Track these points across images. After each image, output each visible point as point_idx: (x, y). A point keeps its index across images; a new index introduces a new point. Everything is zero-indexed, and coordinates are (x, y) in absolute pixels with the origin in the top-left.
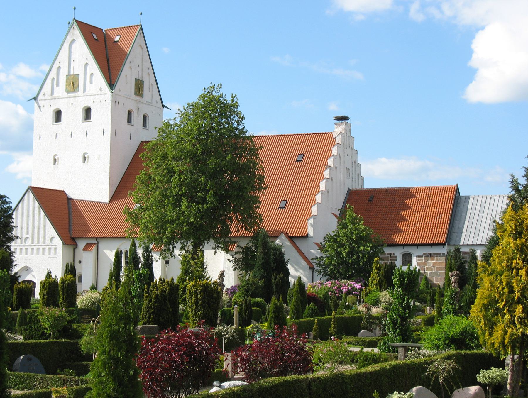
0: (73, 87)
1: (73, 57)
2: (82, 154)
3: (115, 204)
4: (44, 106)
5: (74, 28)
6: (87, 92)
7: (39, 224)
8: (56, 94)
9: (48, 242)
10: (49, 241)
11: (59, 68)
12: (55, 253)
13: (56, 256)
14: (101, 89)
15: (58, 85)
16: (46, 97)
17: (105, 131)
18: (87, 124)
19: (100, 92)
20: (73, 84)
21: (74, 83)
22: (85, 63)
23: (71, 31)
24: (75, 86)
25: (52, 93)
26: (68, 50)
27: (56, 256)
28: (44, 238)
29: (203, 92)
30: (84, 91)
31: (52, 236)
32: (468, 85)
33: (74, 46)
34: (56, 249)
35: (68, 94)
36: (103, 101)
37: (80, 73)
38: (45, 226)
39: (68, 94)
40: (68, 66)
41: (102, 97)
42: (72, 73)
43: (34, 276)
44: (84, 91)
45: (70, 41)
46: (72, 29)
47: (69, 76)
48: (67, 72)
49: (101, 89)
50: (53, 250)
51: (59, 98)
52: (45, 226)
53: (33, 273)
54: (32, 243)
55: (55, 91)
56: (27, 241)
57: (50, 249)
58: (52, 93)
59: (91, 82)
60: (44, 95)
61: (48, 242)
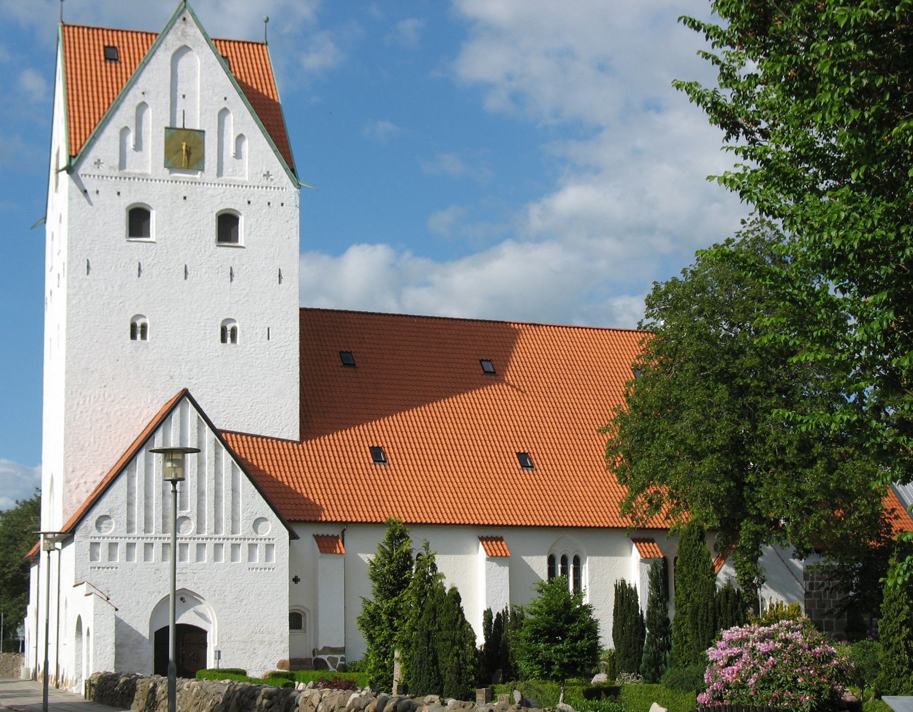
0: (189, 159)
1: (181, 89)
2: (220, 322)
3: (310, 444)
4: (97, 192)
5: (184, 19)
6: (226, 177)
7: (218, 484)
8: (130, 168)
9: (244, 528)
10: (251, 529)
11: (142, 106)
12: (268, 557)
13: (269, 564)
14: (267, 175)
15: (138, 146)
16: (104, 169)
17: (91, 265)
18: (138, 244)
19: (265, 182)
20: (188, 153)
21: (192, 151)
22: (222, 107)
23: (177, 25)
24: (193, 156)
25: (122, 165)
26: (169, 68)
27: (112, 563)
28: (234, 520)
29: (740, 227)
30: (220, 173)
31: (258, 516)
32: (359, 242)
33: (183, 62)
34: (269, 547)
35: (170, 173)
36: (276, 205)
37: (205, 129)
38: (234, 490)
39: (170, 173)
40: (169, 106)
41: (273, 195)
42: (179, 125)
43: (202, 616)
44: (220, 173)
45: (176, 48)
46: (180, 20)
47: (171, 131)
48: (169, 120)
49: (267, 175)
50: (259, 552)
51: (143, 177)
52: (234, 490)
53: (203, 608)
54: (216, 532)
55: (128, 160)
56: (103, 526)
57: (252, 547)
58: (122, 165)
59: (238, 155)
60: (98, 163)
61: (244, 528)
